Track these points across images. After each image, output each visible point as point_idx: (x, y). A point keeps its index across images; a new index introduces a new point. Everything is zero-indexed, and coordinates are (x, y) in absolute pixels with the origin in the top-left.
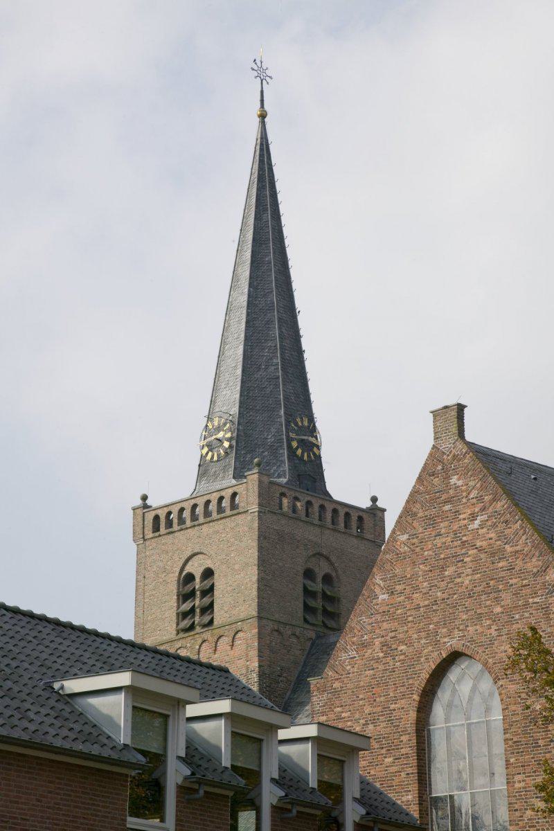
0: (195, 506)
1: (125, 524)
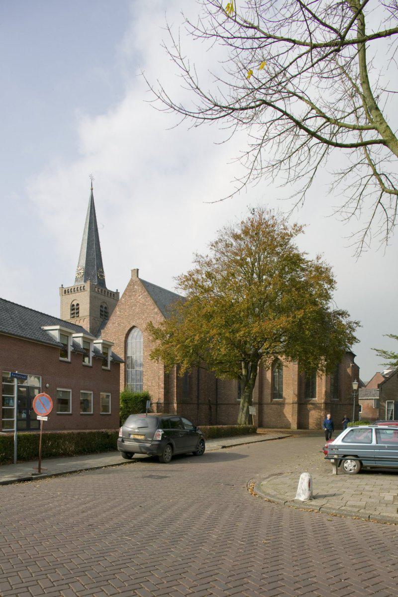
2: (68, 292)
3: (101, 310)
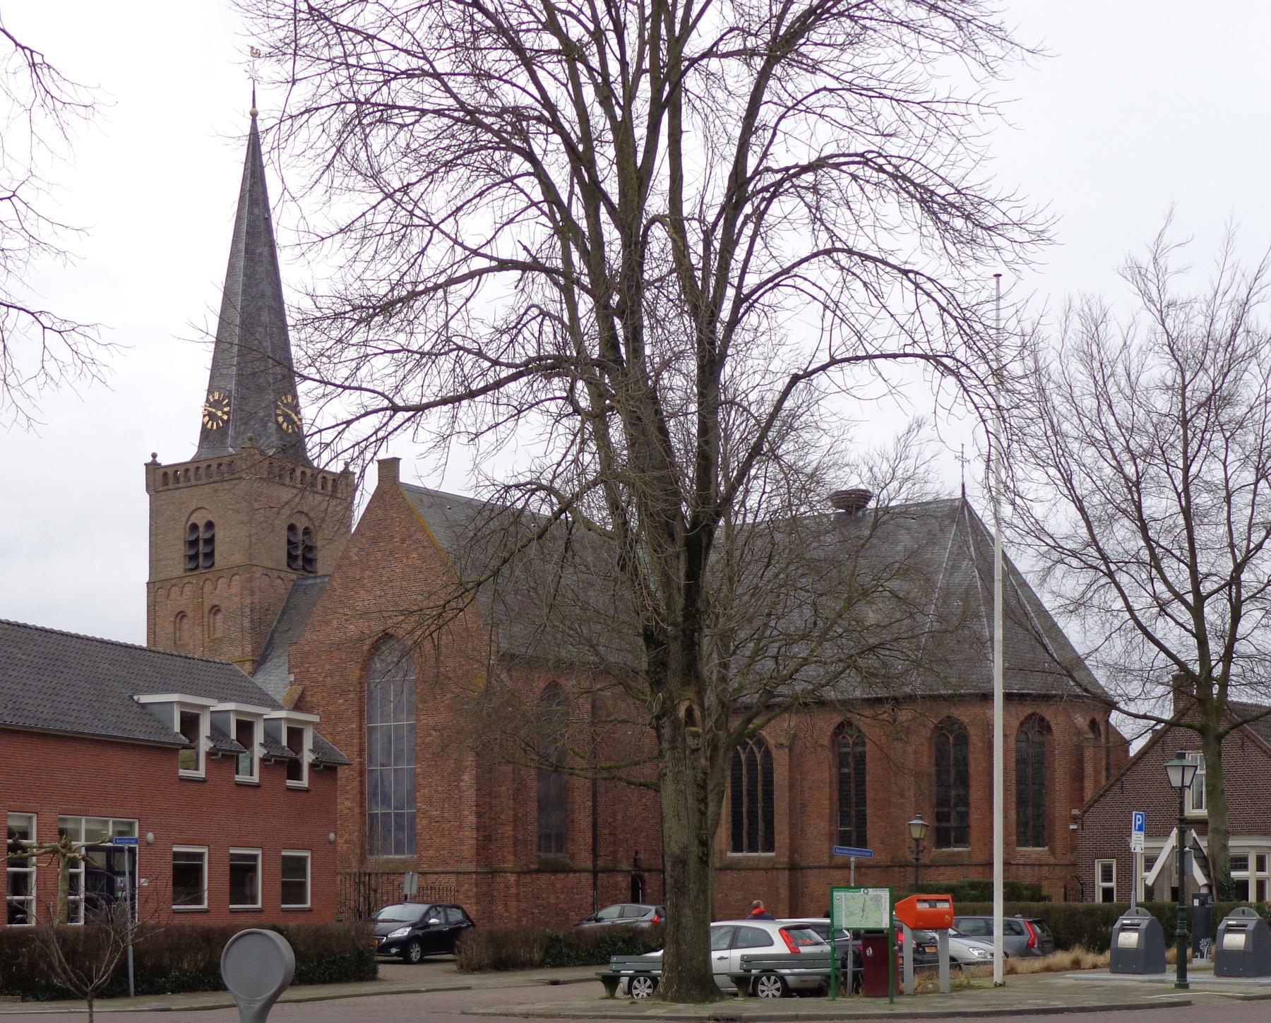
0: (198, 468)
1: (139, 478)
2: (177, 479)
3: (289, 542)
